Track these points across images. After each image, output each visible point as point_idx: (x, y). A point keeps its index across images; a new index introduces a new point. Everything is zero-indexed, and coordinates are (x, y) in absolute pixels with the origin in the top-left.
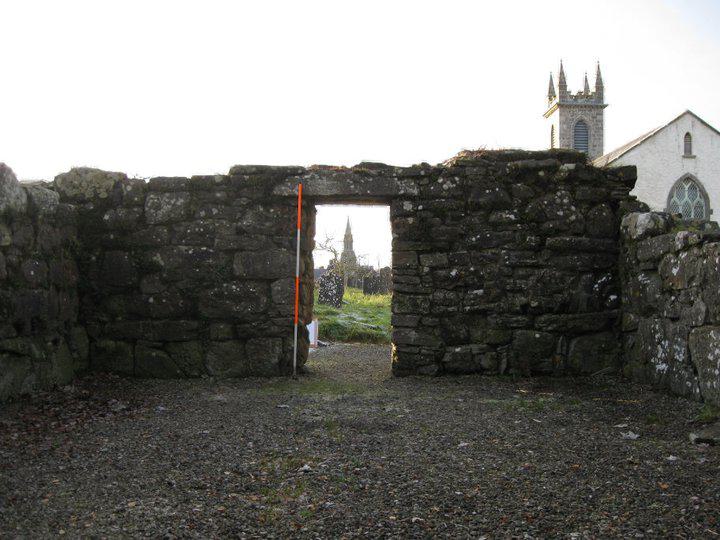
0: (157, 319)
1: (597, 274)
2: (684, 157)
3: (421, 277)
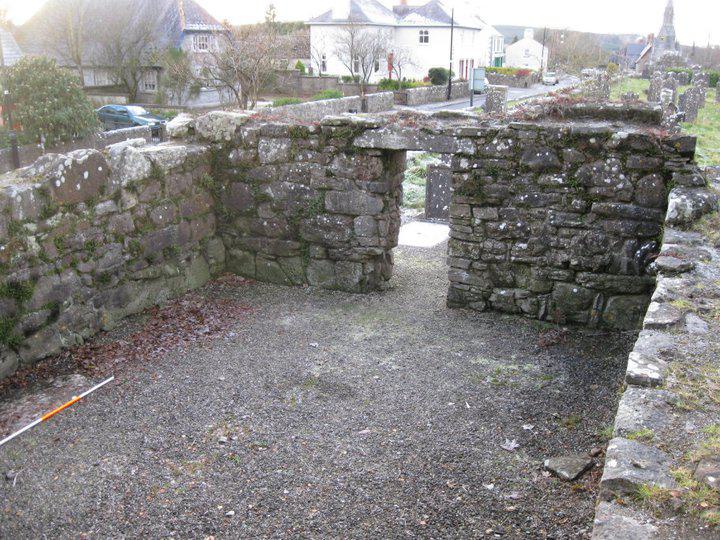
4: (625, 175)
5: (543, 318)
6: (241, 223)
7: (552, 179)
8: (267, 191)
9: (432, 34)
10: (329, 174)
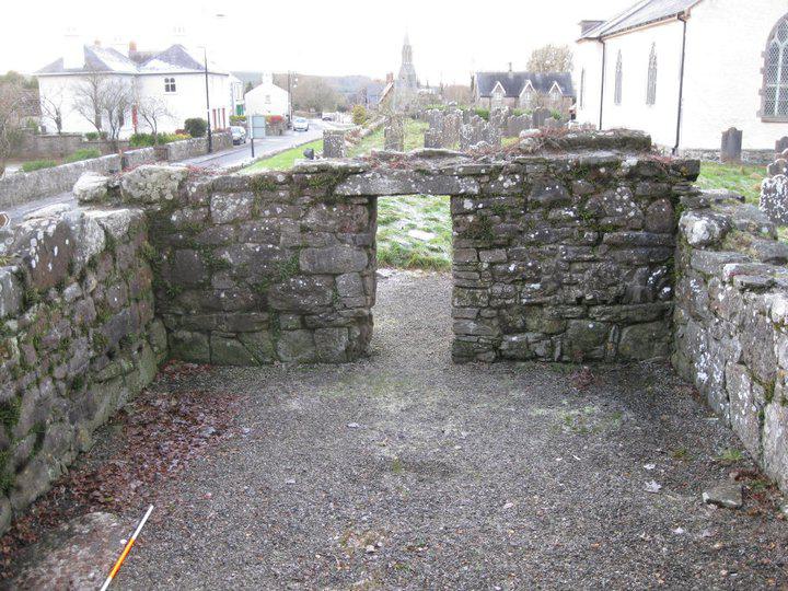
4: (635, 202)
5: (559, 360)
6: (189, 298)
7: (563, 212)
9: (178, 81)
10: (304, 229)
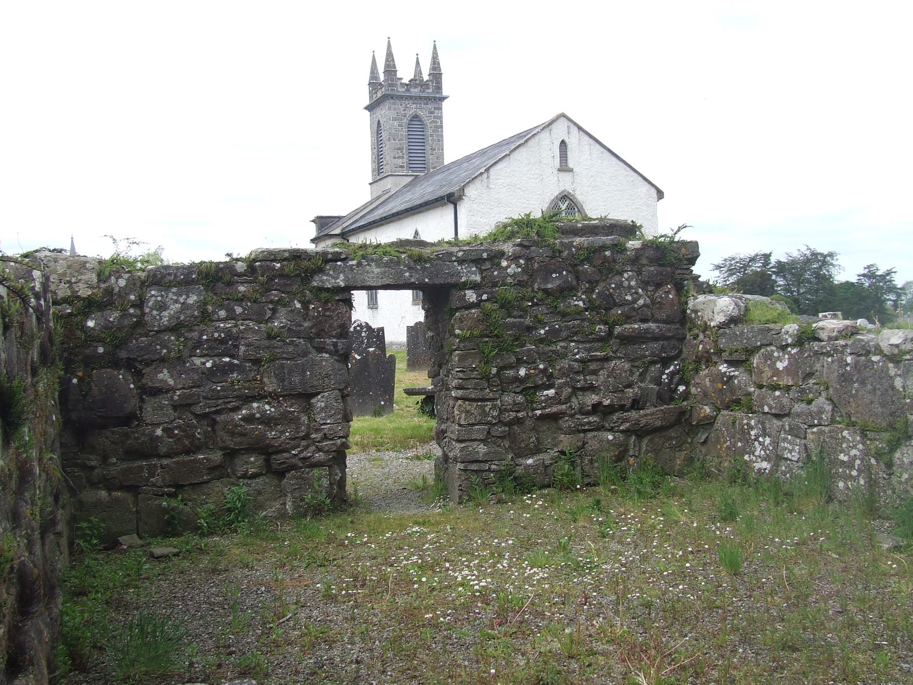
0: (168, 456)
1: (666, 362)
2: (559, 170)
3: (488, 380)
8: (160, 376)
